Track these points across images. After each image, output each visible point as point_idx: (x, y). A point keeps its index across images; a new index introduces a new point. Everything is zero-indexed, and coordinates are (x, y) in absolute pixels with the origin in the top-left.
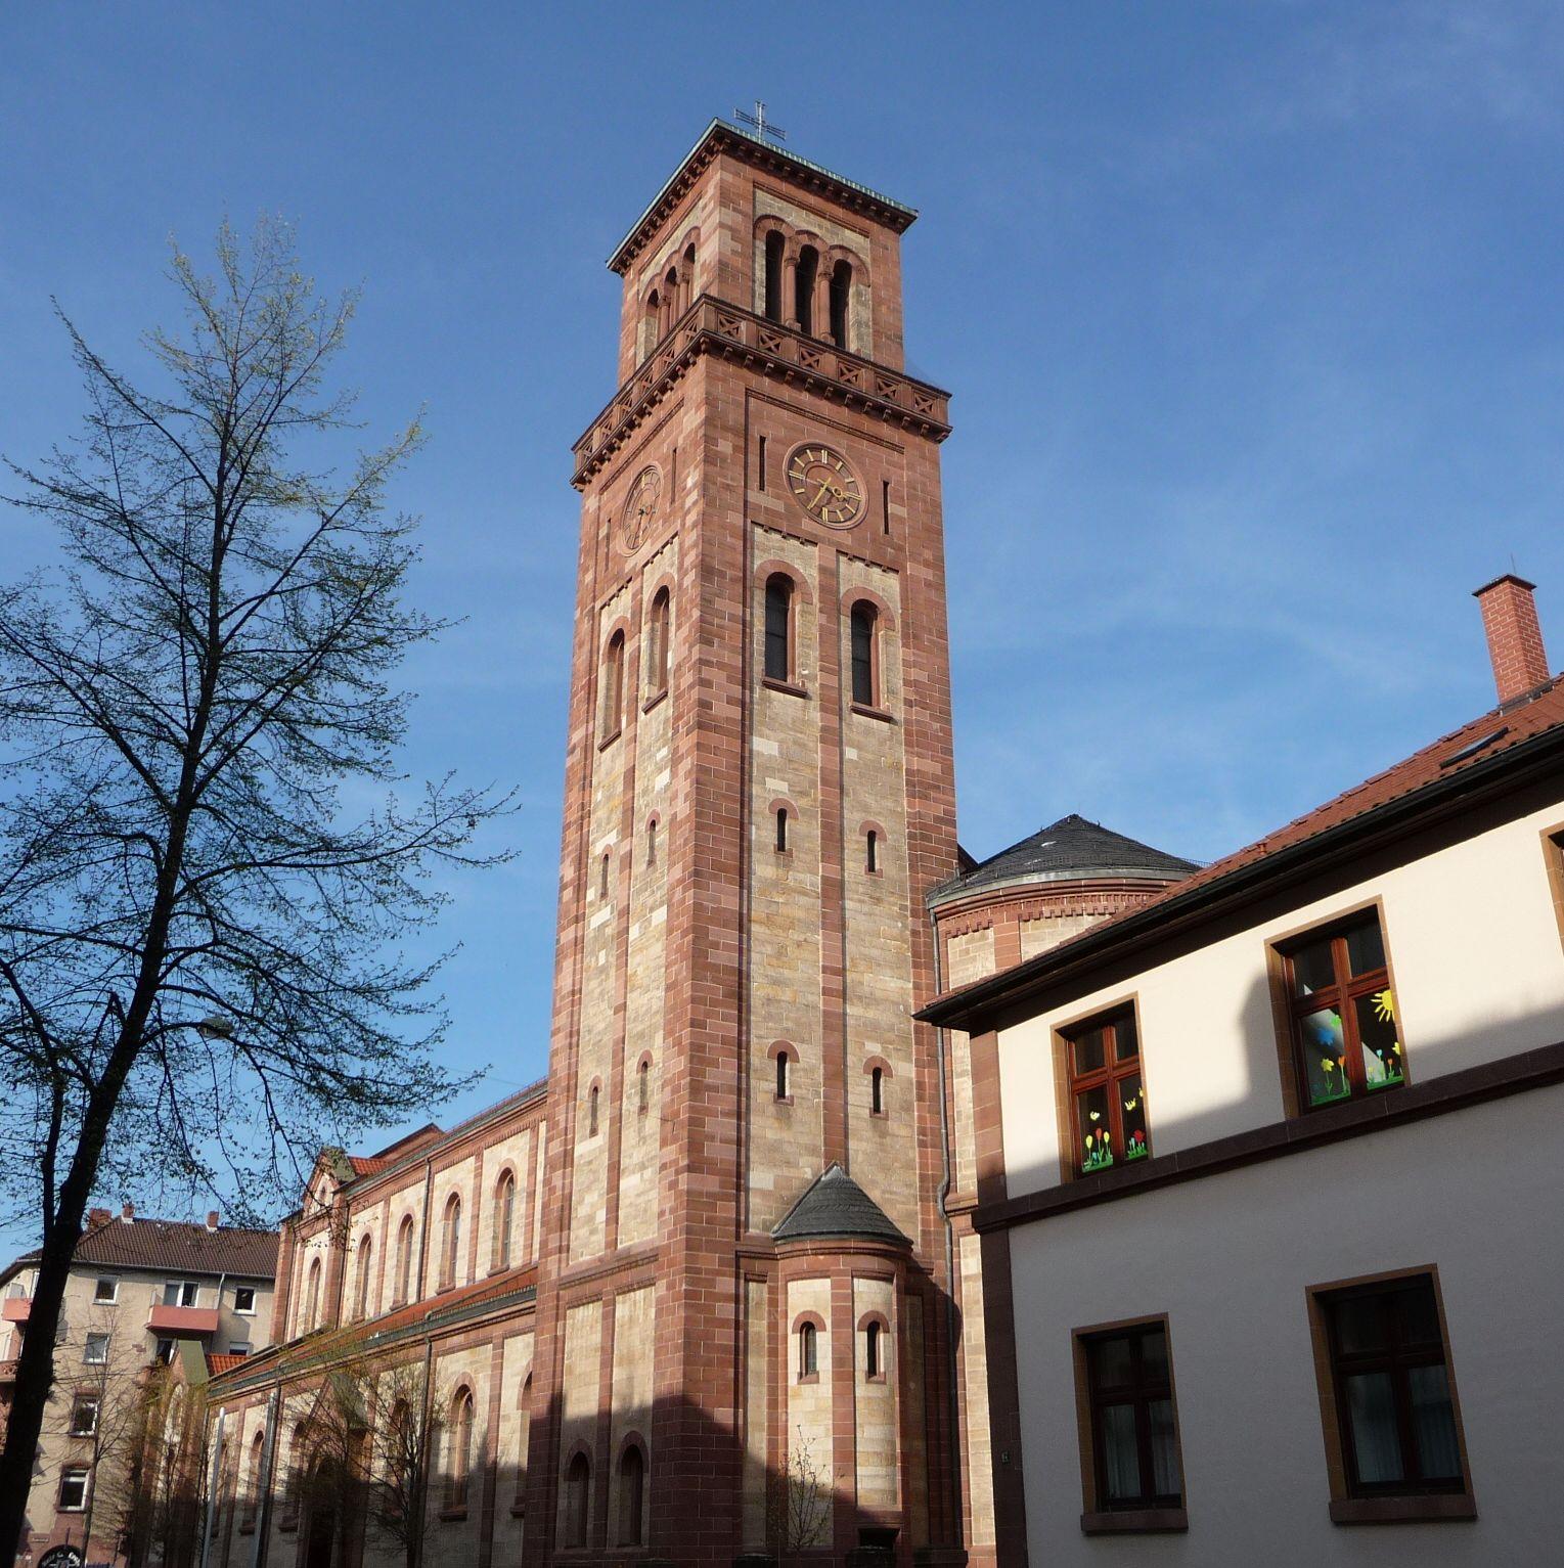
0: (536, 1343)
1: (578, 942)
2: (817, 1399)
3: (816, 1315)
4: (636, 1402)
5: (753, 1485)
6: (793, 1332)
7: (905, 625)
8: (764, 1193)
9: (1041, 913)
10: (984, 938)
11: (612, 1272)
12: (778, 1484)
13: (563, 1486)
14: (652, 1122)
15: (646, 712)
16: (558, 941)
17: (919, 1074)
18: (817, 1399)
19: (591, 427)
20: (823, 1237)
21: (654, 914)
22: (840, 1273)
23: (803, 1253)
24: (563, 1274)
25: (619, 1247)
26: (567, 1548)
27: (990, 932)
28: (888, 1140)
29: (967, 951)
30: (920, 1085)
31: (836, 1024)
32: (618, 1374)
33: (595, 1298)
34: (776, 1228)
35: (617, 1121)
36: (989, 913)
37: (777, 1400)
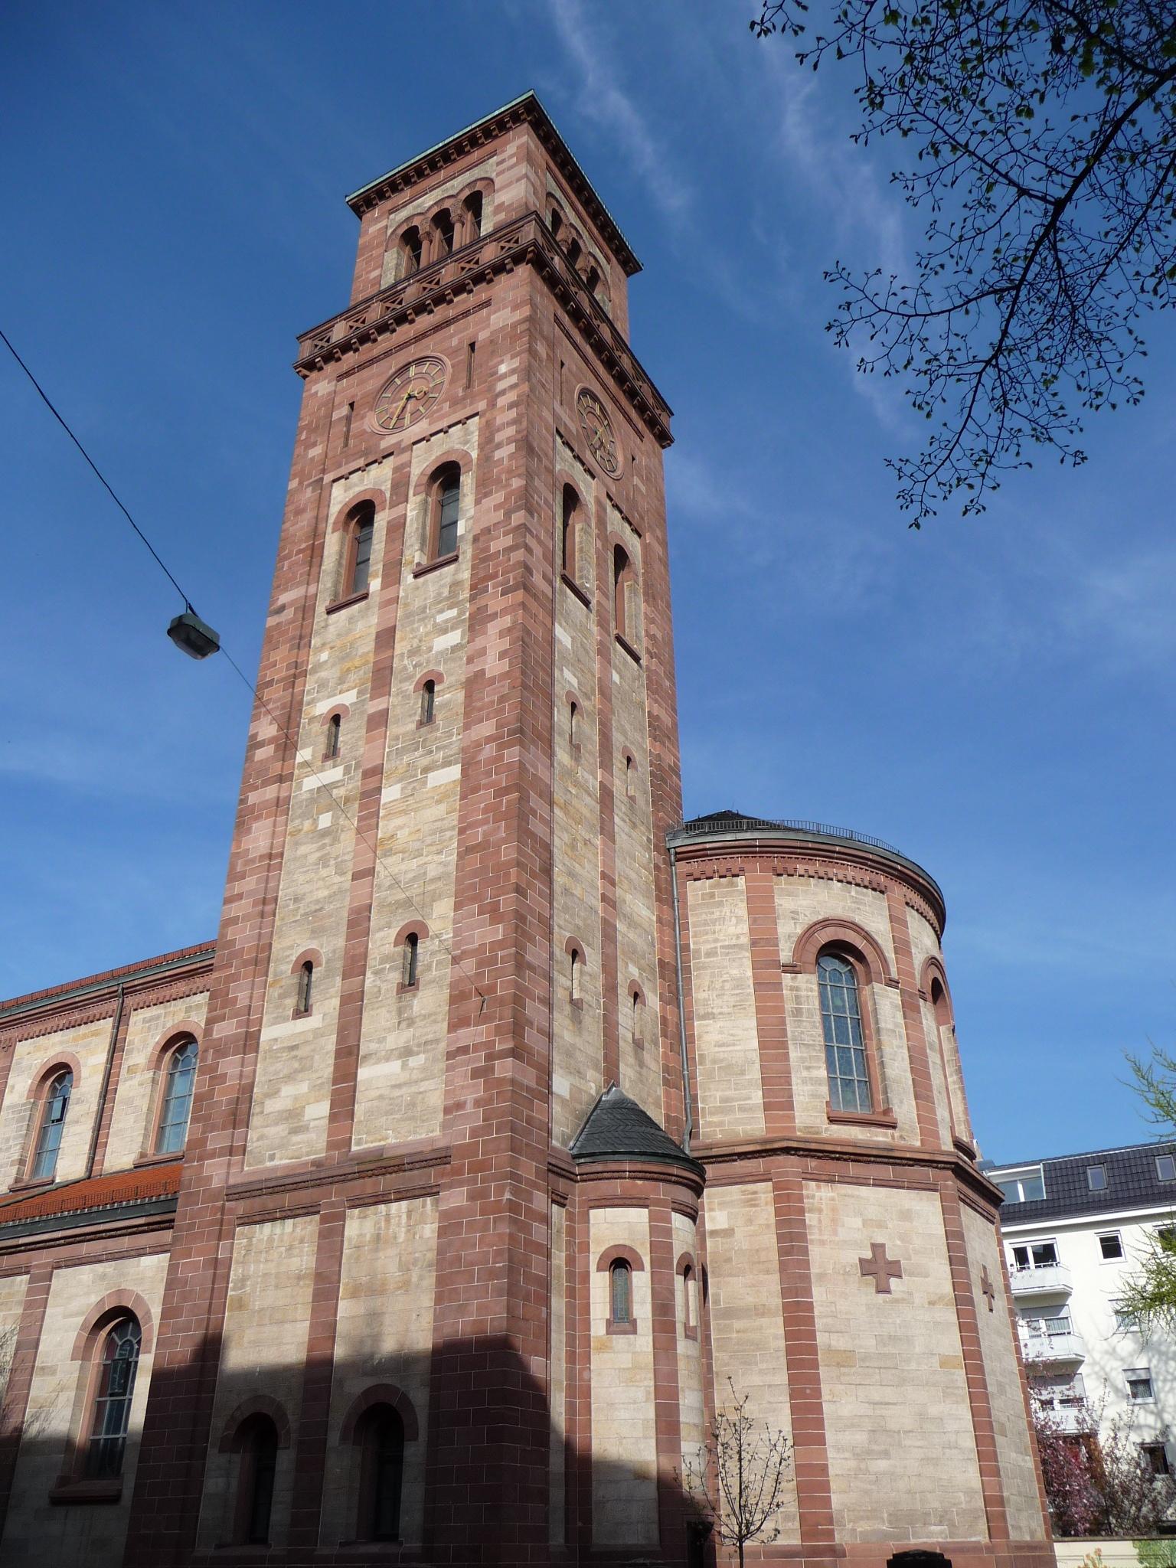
0: (172, 1268)
1: (281, 805)
2: (634, 1353)
3: (631, 1250)
4: (389, 1346)
5: (557, 1462)
6: (599, 1270)
7: (646, 583)
8: (564, 1102)
9: (795, 870)
10: (732, 884)
11: (344, 1178)
12: (581, 1466)
13: (215, 1459)
14: (431, 999)
15: (416, 576)
16: (243, 801)
17: (663, 1009)
18: (634, 1353)
19: (372, 298)
20: (643, 1158)
21: (431, 775)
22: (658, 1202)
23: (617, 1175)
24: (232, 1181)
25: (354, 1148)
26: (219, 1546)
27: (741, 881)
28: (644, 1071)
29: (712, 896)
30: (664, 1020)
31: (609, 934)
32: (346, 1309)
33: (308, 1210)
34: (571, 1144)
35: (353, 1006)
36: (738, 862)
37: (579, 1352)
